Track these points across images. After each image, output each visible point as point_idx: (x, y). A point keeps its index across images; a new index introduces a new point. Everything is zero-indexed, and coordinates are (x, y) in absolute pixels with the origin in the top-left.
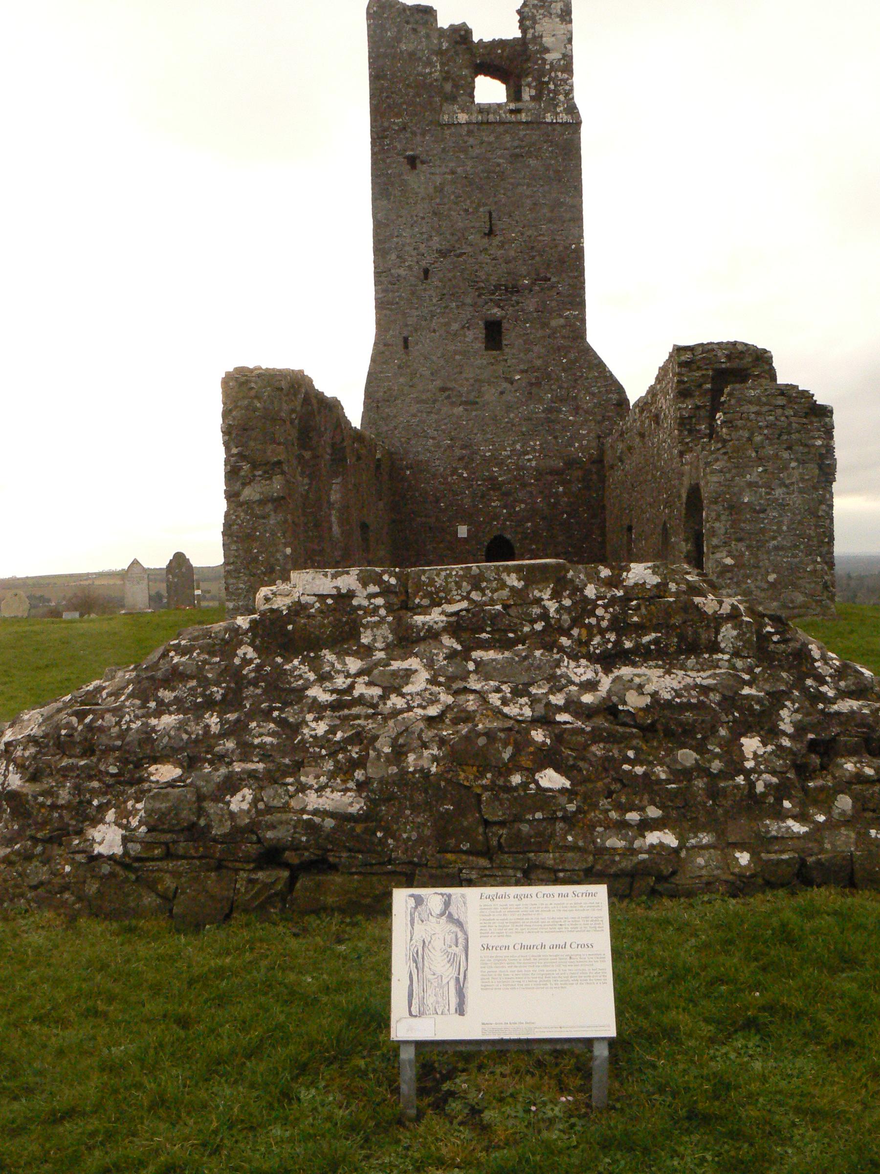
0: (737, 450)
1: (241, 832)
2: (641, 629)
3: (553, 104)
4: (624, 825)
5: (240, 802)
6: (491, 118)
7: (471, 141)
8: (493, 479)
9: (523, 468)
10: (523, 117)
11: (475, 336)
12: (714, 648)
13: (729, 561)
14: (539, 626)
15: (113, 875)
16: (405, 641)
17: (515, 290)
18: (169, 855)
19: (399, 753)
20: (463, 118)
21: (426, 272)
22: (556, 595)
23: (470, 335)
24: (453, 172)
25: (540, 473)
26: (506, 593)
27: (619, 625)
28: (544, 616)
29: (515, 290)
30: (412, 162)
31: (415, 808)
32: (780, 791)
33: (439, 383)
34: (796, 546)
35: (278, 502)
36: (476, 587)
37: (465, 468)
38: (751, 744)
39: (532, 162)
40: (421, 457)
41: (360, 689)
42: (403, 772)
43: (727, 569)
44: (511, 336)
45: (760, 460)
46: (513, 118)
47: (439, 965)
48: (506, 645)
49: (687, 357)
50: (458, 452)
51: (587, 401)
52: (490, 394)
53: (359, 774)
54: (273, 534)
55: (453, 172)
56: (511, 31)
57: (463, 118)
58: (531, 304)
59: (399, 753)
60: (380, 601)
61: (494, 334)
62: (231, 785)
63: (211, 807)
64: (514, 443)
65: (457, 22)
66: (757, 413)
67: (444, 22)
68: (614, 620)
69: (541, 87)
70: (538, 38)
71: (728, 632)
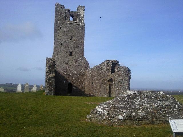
0: (119, 74)
1: (134, 117)
2: (163, 98)
3: (81, 22)
4: (167, 117)
5: (134, 114)
6: (72, 23)
7: (69, 26)
8: (69, 74)
9: (74, 73)
10: (77, 23)
11: (68, 54)
12: (169, 100)
13: (117, 89)
14: (154, 97)
15: (122, 121)
16: (142, 98)
17: (74, 48)
18: (128, 119)
19: (147, 109)
20: (68, 22)
21: (62, 44)
22: (155, 94)
23: (67, 54)
24: (66, 30)
25: (76, 74)
26: (150, 94)
27: (161, 97)
28: (154, 96)
29: (74, 48)
30: (60, 28)
31: (149, 114)
32: (178, 114)
33: (63, 60)
34: (126, 87)
35: (53, 77)
36: (147, 93)
37: (66, 73)
38: (175, 109)
39: (78, 30)
40: (59, 71)
41: (140, 103)
42: (148, 111)
43: (117, 90)
44: (74, 54)
45: (122, 76)
46: (75, 23)
47: (174, 126)
48: (151, 99)
49: (109, 61)
50: (65, 70)
51: (83, 64)
52: (70, 63)
53: (144, 111)
54: (53, 82)
55: (66, 30)
56: (75, 10)
57: (68, 22)
58: (76, 50)
59: (147, 109)
60: (139, 94)
61: (71, 54)
62: (132, 112)
63: (131, 114)
64: (73, 70)
65: (68, 8)
66: (122, 70)
67: (66, 8)
68: (161, 97)
69: (80, 19)
70: (80, 12)
71: (170, 99)
